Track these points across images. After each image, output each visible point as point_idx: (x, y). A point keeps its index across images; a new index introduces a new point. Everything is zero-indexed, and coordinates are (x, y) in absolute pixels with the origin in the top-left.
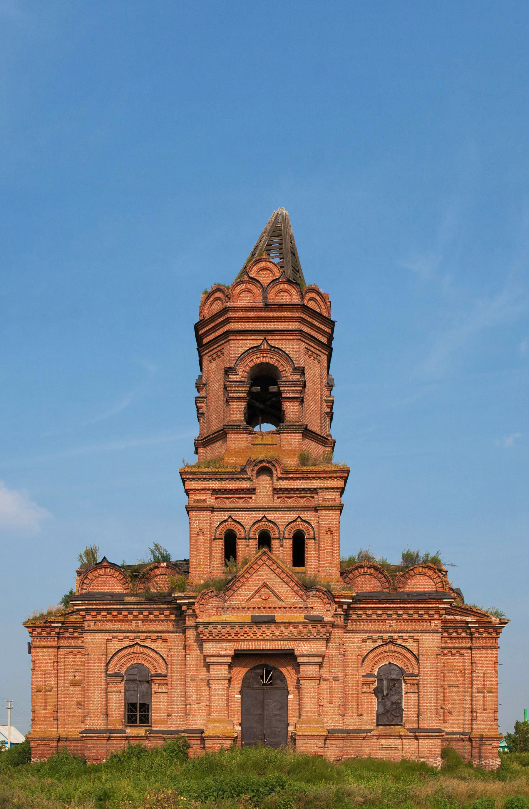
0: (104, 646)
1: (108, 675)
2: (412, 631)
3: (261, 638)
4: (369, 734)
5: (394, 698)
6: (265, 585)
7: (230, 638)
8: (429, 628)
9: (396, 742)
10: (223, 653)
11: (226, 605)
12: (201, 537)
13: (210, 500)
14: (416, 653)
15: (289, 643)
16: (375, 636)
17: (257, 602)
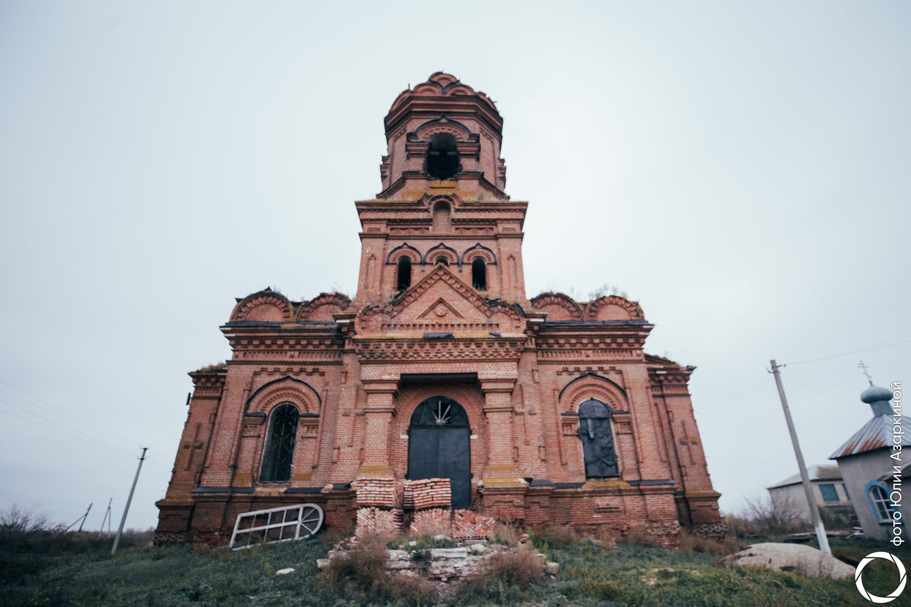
0: (250, 380)
1: (246, 414)
2: (613, 362)
3: (435, 358)
4: (579, 490)
5: (604, 441)
6: (441, 301)
7: (395, 359)
8: (631, 358)
9: (615, 502)
10: (386, 377)
11: (393, 322)
12: (372, 262)
13: (383, 229)
14: (621, 385)
15: (470, 365)
16: (571, 368)
17: (430, 319)
